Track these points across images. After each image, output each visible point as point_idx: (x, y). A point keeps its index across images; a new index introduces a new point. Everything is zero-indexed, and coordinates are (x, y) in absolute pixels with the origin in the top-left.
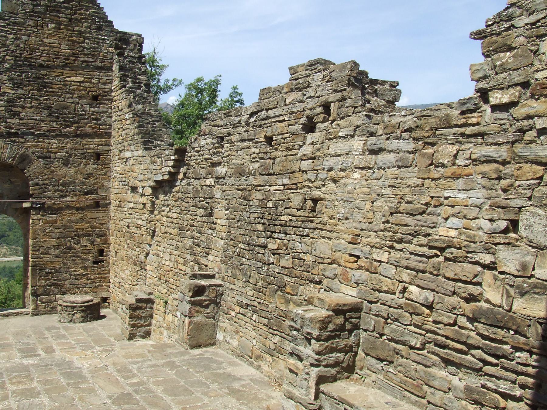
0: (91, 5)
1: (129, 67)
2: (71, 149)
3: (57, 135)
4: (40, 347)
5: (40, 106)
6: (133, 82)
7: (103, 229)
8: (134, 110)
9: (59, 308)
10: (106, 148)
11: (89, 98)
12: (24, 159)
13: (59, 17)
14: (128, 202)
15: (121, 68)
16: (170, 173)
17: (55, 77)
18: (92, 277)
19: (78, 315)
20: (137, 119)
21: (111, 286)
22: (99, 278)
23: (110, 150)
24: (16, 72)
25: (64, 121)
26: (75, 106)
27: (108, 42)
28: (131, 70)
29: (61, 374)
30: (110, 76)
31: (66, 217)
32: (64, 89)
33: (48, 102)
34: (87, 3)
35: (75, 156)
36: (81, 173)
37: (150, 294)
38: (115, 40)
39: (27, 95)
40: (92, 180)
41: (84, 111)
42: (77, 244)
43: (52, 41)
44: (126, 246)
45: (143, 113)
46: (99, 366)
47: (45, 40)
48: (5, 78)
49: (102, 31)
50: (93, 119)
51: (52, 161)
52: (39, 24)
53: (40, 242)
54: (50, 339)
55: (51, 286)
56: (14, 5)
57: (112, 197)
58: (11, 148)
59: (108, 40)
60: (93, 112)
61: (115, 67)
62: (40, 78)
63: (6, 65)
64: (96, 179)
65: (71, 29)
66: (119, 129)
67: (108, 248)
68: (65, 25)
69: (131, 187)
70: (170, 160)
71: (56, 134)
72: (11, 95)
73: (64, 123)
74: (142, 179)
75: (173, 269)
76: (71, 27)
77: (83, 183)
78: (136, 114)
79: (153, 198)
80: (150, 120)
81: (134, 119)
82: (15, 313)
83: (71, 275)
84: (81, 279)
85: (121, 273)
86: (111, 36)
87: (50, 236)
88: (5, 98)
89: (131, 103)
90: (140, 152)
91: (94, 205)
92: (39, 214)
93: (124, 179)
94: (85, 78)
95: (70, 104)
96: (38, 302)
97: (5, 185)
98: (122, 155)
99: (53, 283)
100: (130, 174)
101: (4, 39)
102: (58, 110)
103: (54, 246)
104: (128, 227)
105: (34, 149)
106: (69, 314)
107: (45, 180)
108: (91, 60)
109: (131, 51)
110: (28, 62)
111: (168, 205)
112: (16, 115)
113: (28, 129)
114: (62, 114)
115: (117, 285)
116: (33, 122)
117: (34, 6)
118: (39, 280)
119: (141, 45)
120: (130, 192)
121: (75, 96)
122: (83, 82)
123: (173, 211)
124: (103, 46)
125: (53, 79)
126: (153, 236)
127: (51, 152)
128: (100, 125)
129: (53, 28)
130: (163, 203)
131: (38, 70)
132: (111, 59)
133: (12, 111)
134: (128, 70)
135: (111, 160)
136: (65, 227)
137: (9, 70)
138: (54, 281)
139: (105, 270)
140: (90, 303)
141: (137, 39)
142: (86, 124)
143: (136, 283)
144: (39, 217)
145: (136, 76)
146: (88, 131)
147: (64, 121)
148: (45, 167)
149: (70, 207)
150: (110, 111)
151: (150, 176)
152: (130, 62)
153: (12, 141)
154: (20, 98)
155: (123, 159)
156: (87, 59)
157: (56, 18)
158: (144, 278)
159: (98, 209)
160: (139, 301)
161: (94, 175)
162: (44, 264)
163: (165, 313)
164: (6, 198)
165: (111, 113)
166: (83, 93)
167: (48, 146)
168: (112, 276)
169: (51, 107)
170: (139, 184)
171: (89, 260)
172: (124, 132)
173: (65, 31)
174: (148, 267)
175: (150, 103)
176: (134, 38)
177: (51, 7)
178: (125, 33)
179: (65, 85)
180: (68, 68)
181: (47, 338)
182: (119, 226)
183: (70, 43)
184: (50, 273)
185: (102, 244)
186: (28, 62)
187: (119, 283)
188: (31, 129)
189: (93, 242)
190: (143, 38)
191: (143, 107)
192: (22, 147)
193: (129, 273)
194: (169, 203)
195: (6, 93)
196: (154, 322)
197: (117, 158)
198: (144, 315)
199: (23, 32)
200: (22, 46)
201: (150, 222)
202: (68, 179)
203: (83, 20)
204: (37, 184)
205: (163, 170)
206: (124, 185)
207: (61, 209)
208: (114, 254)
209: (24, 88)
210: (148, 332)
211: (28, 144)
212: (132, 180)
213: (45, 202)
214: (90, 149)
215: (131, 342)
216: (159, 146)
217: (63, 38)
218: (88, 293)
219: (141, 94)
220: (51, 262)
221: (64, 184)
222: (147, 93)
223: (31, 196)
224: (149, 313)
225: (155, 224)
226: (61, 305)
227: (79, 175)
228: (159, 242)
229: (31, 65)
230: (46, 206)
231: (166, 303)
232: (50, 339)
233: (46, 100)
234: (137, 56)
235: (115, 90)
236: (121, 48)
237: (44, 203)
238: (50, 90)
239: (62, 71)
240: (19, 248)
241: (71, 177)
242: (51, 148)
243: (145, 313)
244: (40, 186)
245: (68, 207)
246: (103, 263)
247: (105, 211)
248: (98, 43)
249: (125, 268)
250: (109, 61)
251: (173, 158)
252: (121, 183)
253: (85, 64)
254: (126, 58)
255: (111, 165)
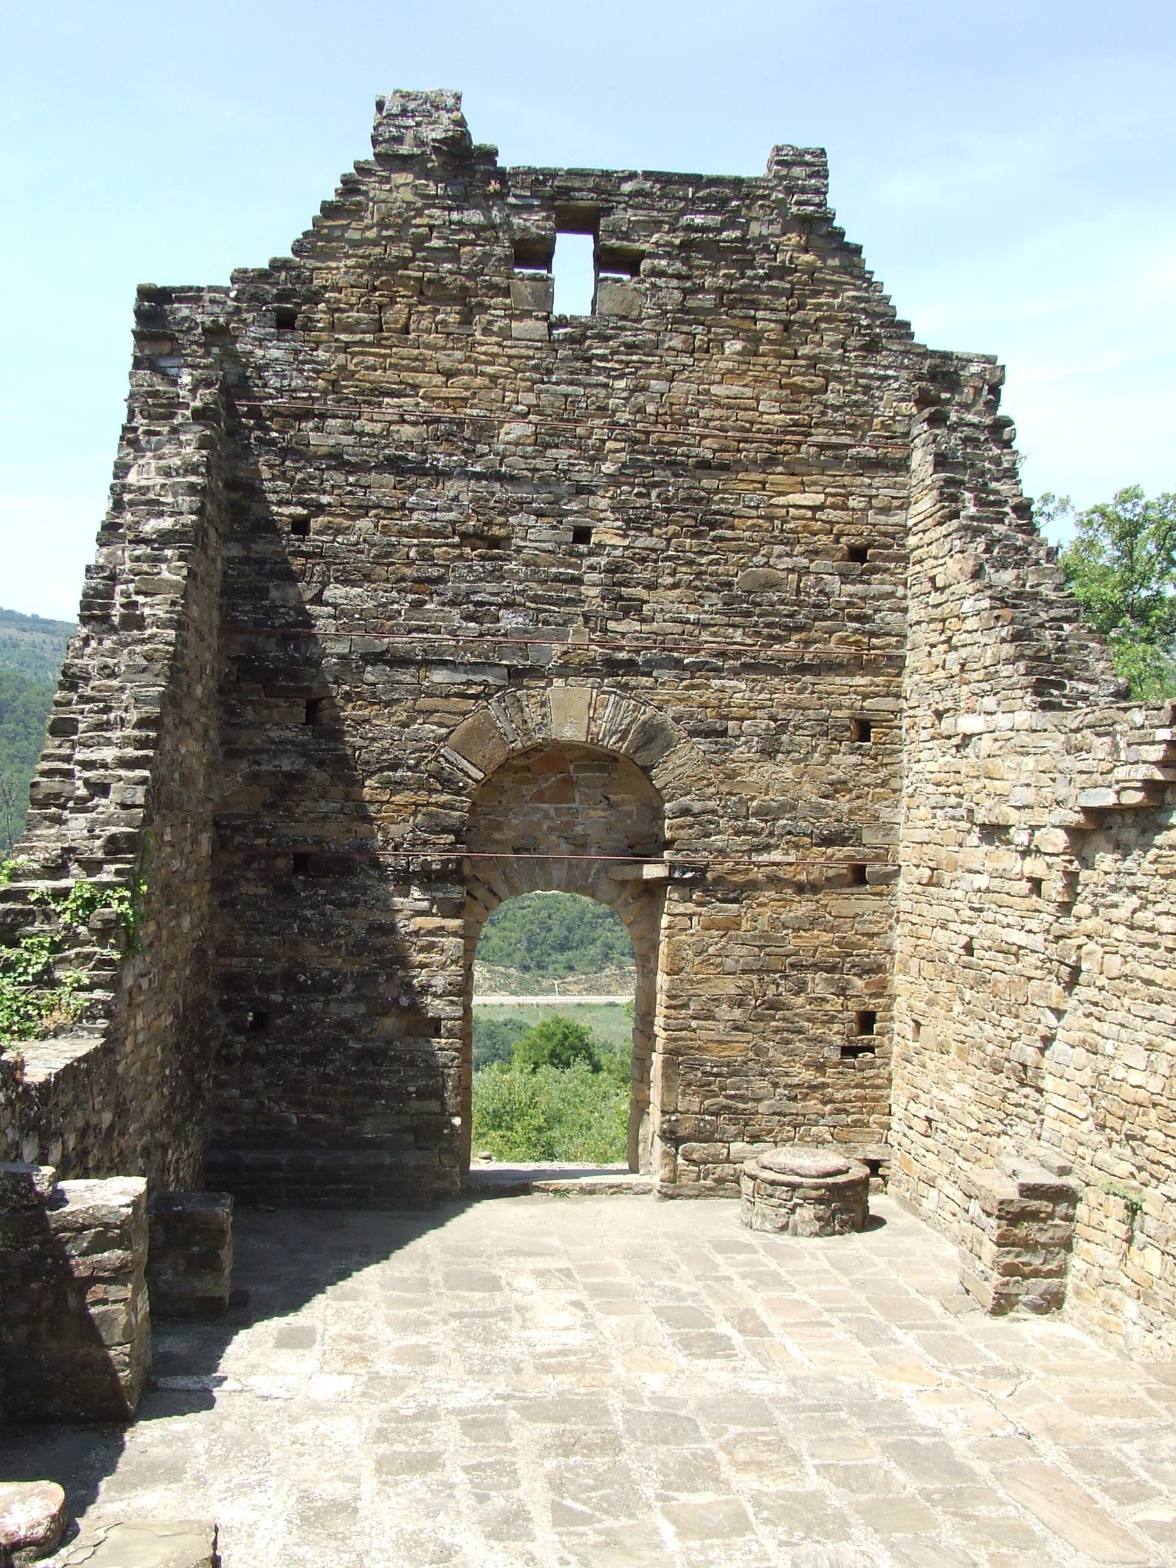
0: (846, 278)
1: (965, 455)
2: (787, 706)
3: (747, 667)
4: (718, 1309)
5: (698, 583)
6: (980, 503)
7: (870, 952)
8: (990, 587)
9: (747, 1185)
10: (889, 703)
11: (839, 555)
12: (652, 737)
13: (754, 320)
14: (970, 871)
15: (941, 462)
16: (1149, 785)
17: (742, 495)
18: (838, 1096)
19: (807, 1212)
20: (1007, 613)
21: (894, 1126)
22: (858, 1098)
23: (901, 711)
24: (633, 485)
25: (768, 625)
26: (800, 581)
27: (896, 386)
28: (972, 466)
29: (885, 1448)
30: (904, 486)
31: (768, 912)
32: (767, 530)
33: (721, 569)
34: (835, 273)
35: (797, 727)
36: (813, 780)
37: (1064, 1171)
38: (919, 378)
39: (663, 551)
40: (844, 803)
41: (826, 594)
42: (797, 994)
43: (735, 390)
44: (958, 1008)
45: (1018, 595)
46: (1000, 1433)
47: (714, 389)
48: (604, 503)
49: (879, 352)
50: (852, 618)
51: (730, 744)
52: (697, 343)
53: (691, 982)
54: (739, 1284)
55: (717, 1114)
56: (631, 296)
57: (905, 855)
58: (617, 705)
59: (896, 379)
60: (851, 596)
61: (921, 460)
62: (698, 501)
63: (608, 468)
64: (858, 797)
65: (790, 351)
66: (933, 646)
67: (888, 1008)
68: (770, 342)
69: (983, 826)
70: (1153, 743)
71: (743, 664)
72: (618, 552)
73: (765, 631)
74: (1031, 801)
75: (1164, 1101)
76: (787, 345)
77: (820, 810)
78: (1001, 599)
79: (1071, 862)
80: (1043, 614)
81: (996, 613)
82: (610, 1187)
83: (775, 1085)
84: (804, 1099)
85: (935, 1091)
86: (907, 368)
87: (721, 964)
88: (603, 561)
89: (981, 565)
90: (1023, 718)
91: (850, 877)
92: (690, 900)
93: (953, 800)
94: (827, 495)
95: (783, 575)
96: (680, 1160)
97: (592, 812)
98: (946, 725)
99: (724, 1107)
100: (977, 785)
101: (603, 392)
102: (750, 592)
103: (730, 997)
104: (969, 949)
105: (681, 708)
106: (780, 1206)
107: (710, 798)
108: (847, 440)
109: (966, 407)
110: (668, 454)
111: (1133, 890)
112: (631, 608)
113: (664, 649)
114: (759, 604)
115: (922, 1126)
116: (678, 628)
117: (686, 292)
118: (684, 1094)
119: (995, 390)
120: (976, 842)
121: (798, 549)
122: (821, 508)
123: (1160, 907)
124: (881, 399)
125: (737, 502)
126: (1072, 983)
127: (726, 718)
128: (872, 634)
129: (738, 353)
130: (1111, 879)
131: (693, 477)
132: (906, 434)
133: (621, 597)
134: (963, 466)
135: (901, 741)
136: (764, 941)
137: (614, 480)
138: (725, 1102)
139: (877, 1076)
140: (841, 1179)
141: (985, 370)
142: (831, 634)
143: (999, 1127)
144: (691, 907)
145: (985, 484)
146: (830, 650)
147: (768, 625)
148: (711, 762)
149: (780, 880)
150: (900, 591)
151: (1062, 791)
152: (966, 441)
153: (618, 685)
154: (643, 560)
155: (949, 737)
156: (834, 440)
157: (747, 324)
158: (1032, 1115)
159: (862, 889)
160: (1029, 1191)
161: (850, 785)
162: (699, 1049)
163: (1129, 1241)
164: (593, 850)
165: (905, 597)
166: (824, 540)
167: (721, 700)
168: (898, 1096)
169: (729, 585)
170: (1014, 817)
171: (830, 1043)
172: (953, 655)
173: (772, 361)
174: (1048, 1083)
175: (1037, 563)
176: (974, 368)
177: (731, 291)
178: (946, 356)
179: (771, 519)
180: (780, 469)
181: (729, 1279)
182: (930, 943)
183: (785, 392)
184: (717, 1075)
185: (871, 996)
186: (668, 454)
187: (929, 1120)
188: (671, 650)
189: (844, 989)
190: (1003, 367)
191: (1018, 578)
192: (646, 703)
193: (969, 1093)
194: (1139, 880)
195: (605, 546)
196: (1076, 1262)
197: (924, 735)
198: (1043, 1238)
199: (653, 370)
200: (650, 409)
201: (1058, 938)
202: (774, 798)
203: (823, 325)
204: (685, 812)
205: (1121, 773)
206: (953, 818)
207: (753, 885)
208: (909, 1032)
209: (656, 531)
210: (1057, 1293)
211: (662, 694)
212: (988, 803)
213: (707, 866)
214: (840, 707)
215: (1001, 1322)
216: (1084, 696)
217: (765, 381)
218: (824, 1142)
219: (1007, 537)
220: (720, 1042)
221: (763, 813)
222: (1024, 532)
223: (668, 844)
224: (1060, 1233)
225: (1080, 947)
226: (753, 1178)
227: (807, 787)
228: (1096, 1004)
229: (675, 463)
230: (709, 875)
231: (1133, 1209)
232: (739, 1284)
233: (716, 563)
234: (988, 421)
235: (921, 527)
236: (936, 401)
237: (704, 870)
238: (729, 534)
239: (761, 477)
240: (512, 971)
241: (784, 792)
242: (728, 706)
243: (1050, 1233)
244: (694, 815)
245: (774, 881)
246: (870, 1055)
247: (880, 894)
248: (867, 389)
249: (952, 1076)
250: (899, 441)
251: (1164, 734)
252: (939, 812)
253: (829, 453)
254: (955, 430)
255: (904, 756)
